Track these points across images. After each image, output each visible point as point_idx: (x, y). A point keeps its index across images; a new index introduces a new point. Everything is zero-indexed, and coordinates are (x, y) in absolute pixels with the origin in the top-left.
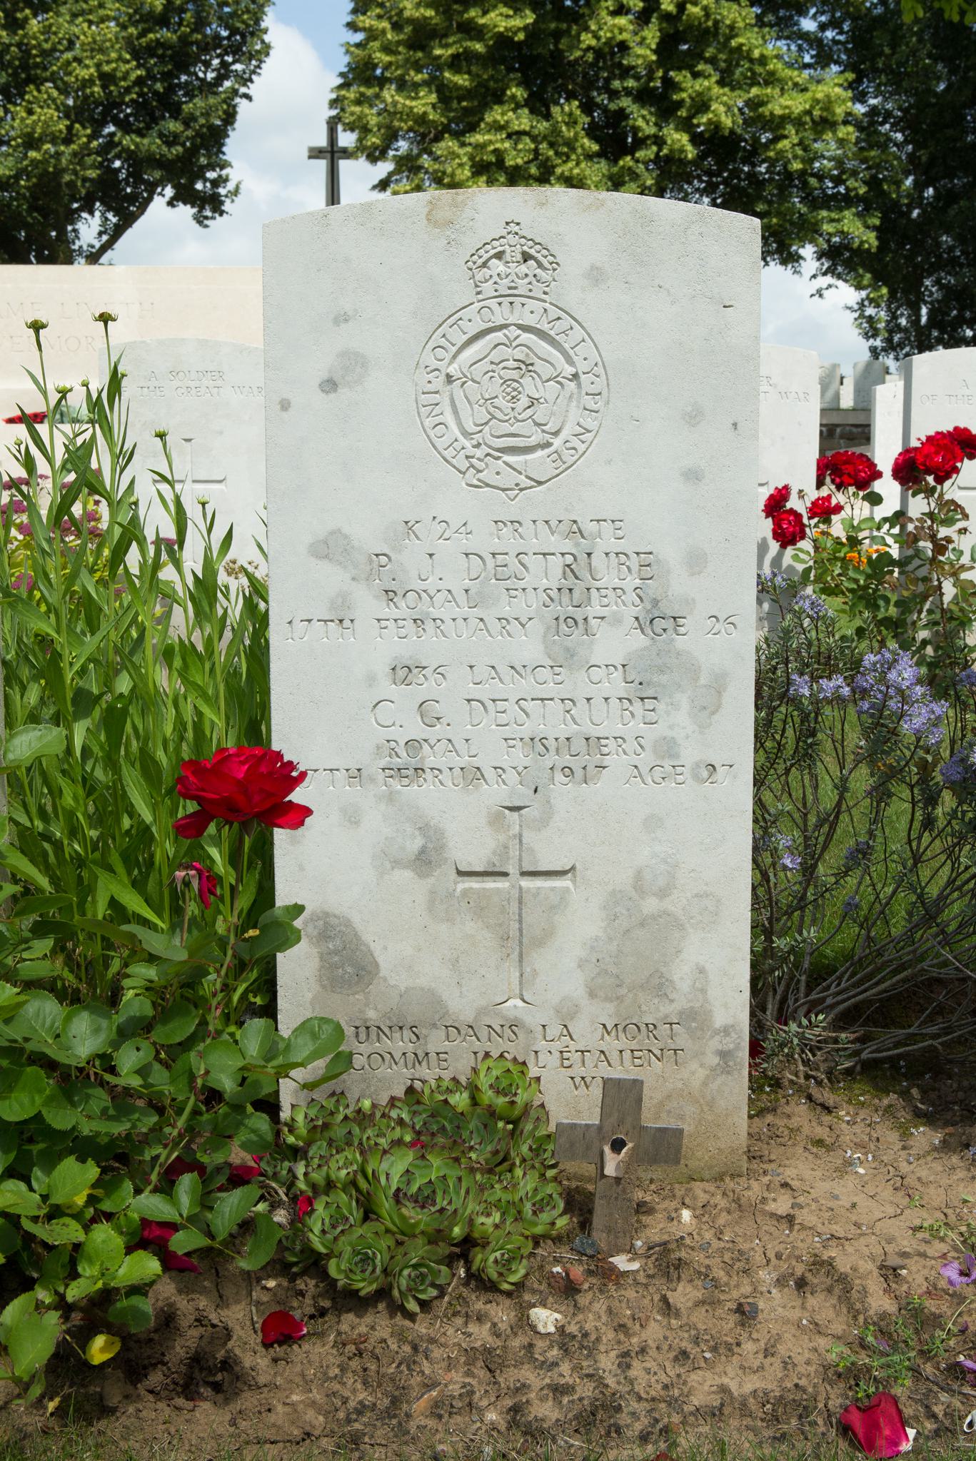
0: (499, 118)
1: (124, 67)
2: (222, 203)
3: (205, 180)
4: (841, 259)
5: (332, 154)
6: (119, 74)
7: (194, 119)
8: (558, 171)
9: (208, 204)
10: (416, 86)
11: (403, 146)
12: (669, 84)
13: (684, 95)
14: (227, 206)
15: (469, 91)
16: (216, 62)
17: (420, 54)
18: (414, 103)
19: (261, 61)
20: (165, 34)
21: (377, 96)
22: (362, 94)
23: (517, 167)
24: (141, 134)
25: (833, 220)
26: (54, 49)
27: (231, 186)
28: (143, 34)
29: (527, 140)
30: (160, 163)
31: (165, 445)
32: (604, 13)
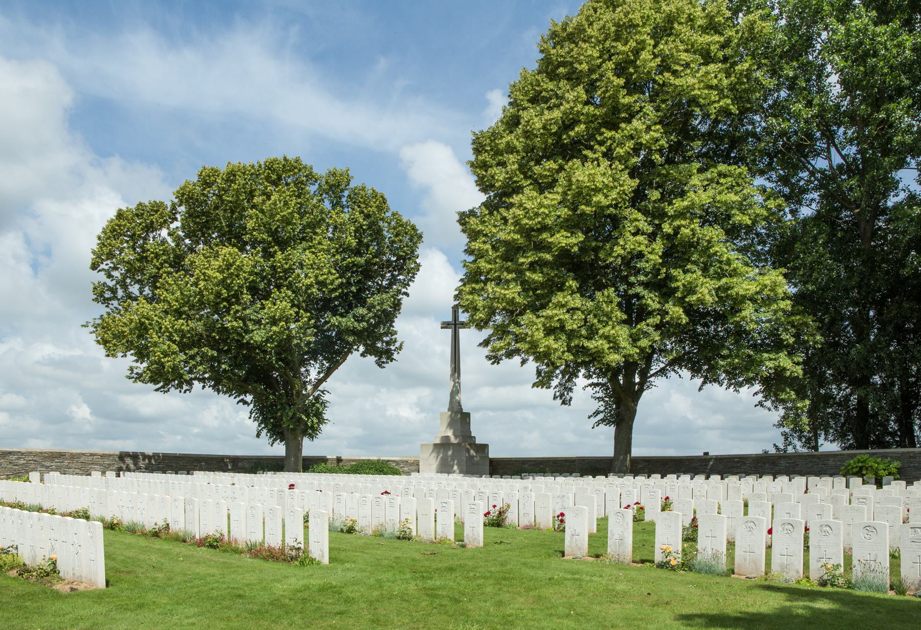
0: (561, 300)
1: (331, 277)
2: (393, 354)
3: (383, 342)
4: (774, 385)
5: (454, 325)
6: (328, 281)
7: (374, 307)
8: (601, 332)
9: (662, 478)
10: (507, 282)
11: (499, 319)
12: (669, 278)
13: (679, 284)
14: (395, 356)
15: (542, 284)
16: (389, 275)
17: (510, 264)
18: (507, 292)
19: (414, 274)
20: (361, 260)
21: (483, 289)
22: (474, 289)
23: (572, 331)
24: (342, 316)
25: (771, 359)
26: (290, 268)
27: (397, 345)
28: (344, 259)
29: (580, 313)
30: (353, 332)
31: (455, 392)
32: (628, 234)
